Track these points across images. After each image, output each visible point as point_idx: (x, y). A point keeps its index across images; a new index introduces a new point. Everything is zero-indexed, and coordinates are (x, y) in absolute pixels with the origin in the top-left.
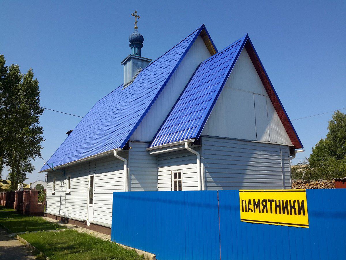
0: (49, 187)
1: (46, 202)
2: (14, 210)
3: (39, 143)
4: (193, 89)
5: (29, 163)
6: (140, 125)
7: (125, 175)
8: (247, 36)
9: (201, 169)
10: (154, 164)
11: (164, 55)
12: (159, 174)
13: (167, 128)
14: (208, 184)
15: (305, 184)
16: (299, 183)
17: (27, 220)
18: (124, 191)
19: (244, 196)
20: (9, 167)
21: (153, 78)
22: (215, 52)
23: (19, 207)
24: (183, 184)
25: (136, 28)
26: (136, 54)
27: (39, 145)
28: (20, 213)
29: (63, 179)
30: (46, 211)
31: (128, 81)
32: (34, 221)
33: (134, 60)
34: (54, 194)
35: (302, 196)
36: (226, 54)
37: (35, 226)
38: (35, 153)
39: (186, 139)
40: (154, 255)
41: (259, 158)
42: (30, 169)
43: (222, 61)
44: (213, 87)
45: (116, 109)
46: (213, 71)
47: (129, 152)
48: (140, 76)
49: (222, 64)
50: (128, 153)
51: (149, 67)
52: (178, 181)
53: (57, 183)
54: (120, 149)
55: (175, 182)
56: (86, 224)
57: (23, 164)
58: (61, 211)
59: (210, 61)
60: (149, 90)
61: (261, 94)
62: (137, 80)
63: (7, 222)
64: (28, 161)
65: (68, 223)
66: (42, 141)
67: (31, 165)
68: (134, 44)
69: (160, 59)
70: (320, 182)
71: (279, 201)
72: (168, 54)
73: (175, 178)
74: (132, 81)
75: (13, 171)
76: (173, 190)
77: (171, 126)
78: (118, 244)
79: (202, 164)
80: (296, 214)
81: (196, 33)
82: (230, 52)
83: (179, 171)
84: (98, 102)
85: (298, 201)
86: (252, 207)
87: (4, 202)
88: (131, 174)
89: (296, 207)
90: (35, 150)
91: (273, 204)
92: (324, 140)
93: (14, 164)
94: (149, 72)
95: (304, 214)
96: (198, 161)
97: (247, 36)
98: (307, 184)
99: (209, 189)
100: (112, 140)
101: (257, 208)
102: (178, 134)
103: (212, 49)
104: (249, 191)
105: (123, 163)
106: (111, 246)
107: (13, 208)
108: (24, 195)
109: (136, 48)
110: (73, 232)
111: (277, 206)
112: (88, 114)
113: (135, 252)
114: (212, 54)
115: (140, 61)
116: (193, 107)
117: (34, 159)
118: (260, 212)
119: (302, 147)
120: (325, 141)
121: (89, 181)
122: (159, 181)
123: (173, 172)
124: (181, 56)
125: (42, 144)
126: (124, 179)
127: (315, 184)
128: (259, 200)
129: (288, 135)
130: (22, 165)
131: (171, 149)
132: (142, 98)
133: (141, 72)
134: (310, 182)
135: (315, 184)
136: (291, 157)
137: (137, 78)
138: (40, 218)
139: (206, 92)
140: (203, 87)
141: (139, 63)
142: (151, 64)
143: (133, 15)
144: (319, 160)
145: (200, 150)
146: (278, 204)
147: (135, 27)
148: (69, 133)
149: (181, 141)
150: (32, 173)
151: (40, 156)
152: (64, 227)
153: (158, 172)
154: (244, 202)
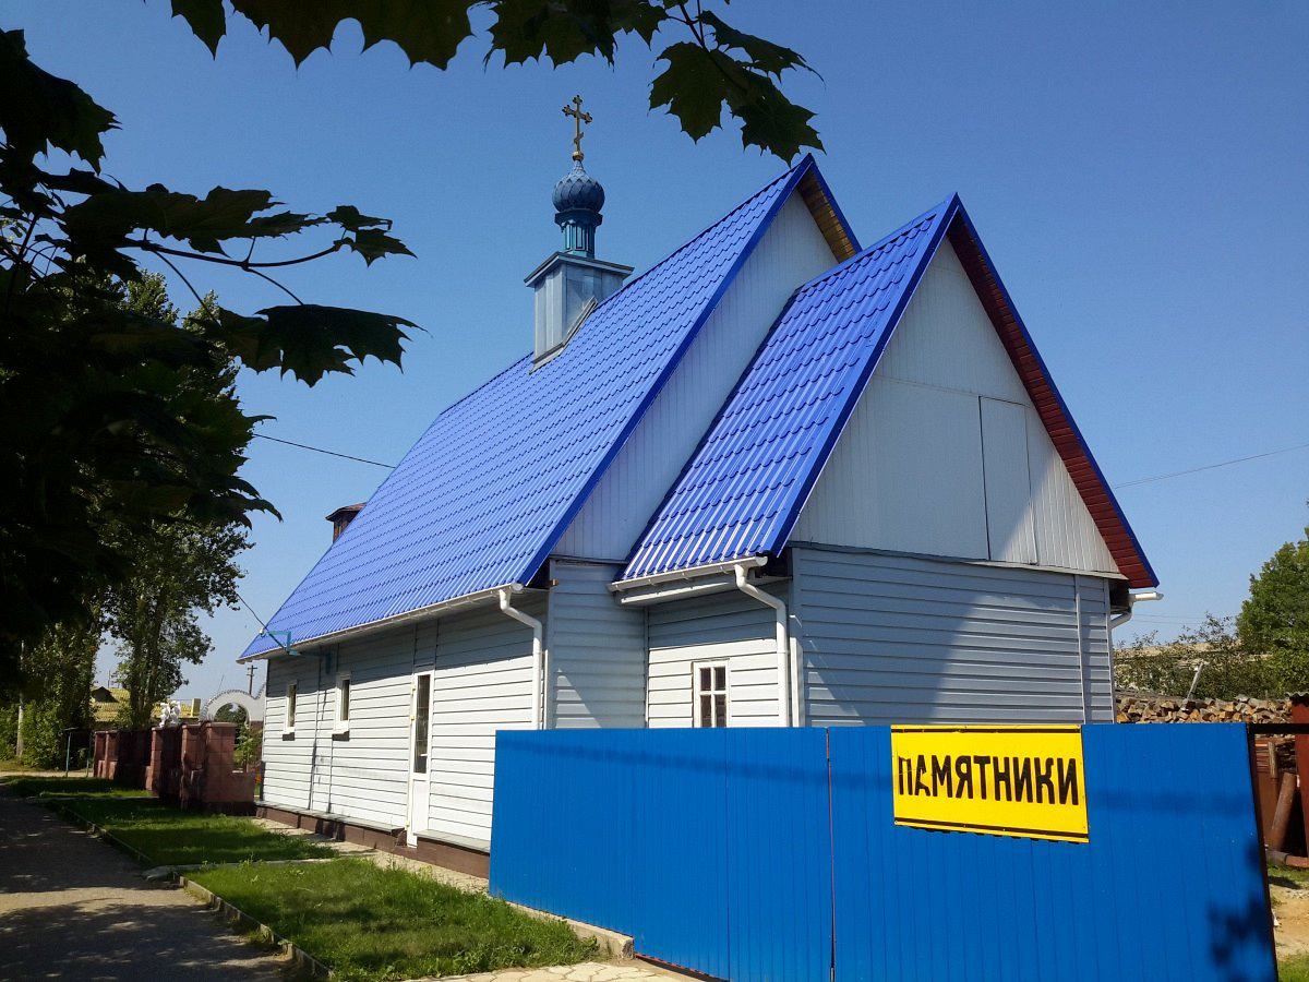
0: (273, 713)
1: (263, 764)
2: (148, 792)
3: (231, 553)
4: (828, 336)
5: (194, 627)
6: (587, 504)
7: (535, 674)
8: (956, 201)
9: (789, 655)
10: (637, 637)
11: (673, 256)
12: (652, 671)
13: (669, 518)
14: (815, 709)
15: (1188, 713)
16: (1167, 710)
17: (199, 826)
18: (533, 727)
19: (907, 745)
20: (120, 641)
21: (662, 297)
22: (849, 248)
23: (163, 783)
24: (731, 709)
25: (578, 158)
26: (578, 249)
27: (230, 562)
28: (168, 801)
29: (323, 685)
30: (261, 798)
31: (551, 345)
32: (222, 831)
33: (571, 270)
34: (290, 737)
35: (1068, 747)
36: (884, 260)
37: (231, 847)
38: (215, 591)
39: (741, 554)
40: (628, 938)
41: (992, 621)
42: (195, 647)
43: (870, 285)
44: (836, 377)
45: (507, 445)
46: (875, 283)
47: (560, 594)
48: (592, 326)
49: (869, 293)
50: (544, 599)
51: (621, 298)
52: (716, 696)
53: (301, 699)
54: (519, 588)
55: (706, 701)
56: (403, 842)
57: (172, 631)
58: (315, 797)
59: (829, 282)
60: (619, 384)
61: (1004, 398)
62: (581, 341)
63: (133, 831)
64: (188, 618)
65: (341, 838)
66: (241, 550)
67: (198, 633)
68: (573, 214)
69: (659, 270)
70: (1242, 708)
71: (1007, 760)
72: (687, 255)
73: (706, 685)
74: (561, 346)
75: (137, 654)
76: (698, 725)
77: (690, 508)
78: (513, 905)
79: (793, 641)
80: (1052, 801)
81: (782, 185)
82: (897, 253)
83: (719, 664)
84: (447, 414)
85: (1060, 761)
86: (927, 779)
87: (108, 764)
88: (555, 669)
89: (1054, 779)
90: (217, 579)
91: (989, 768)
92: (1296, 546)
93: (142, 633)
94: (620, 314)
95: (1075, 802)
96: (780, 629)
97: (956, 201)
98: (1194, 714)
99: (816, 723)
100: (514, 528)
101: (942, 783)
102: (715, 540)
103: (839, 241)
104: (920, 731)
105: (528, 633)
106: (490, 909)
107: (143, 787)
108: (184, 742)
109: (579, 229)
110: (359, 865)
111: (999, 777)
112: (410, 456)
113: (568, 929)
114: (840, 256)
115: (592, 272)
116: (767, 443)
117: (210, 610)
118: (950, 795)
119: (1154, 583)
120: (1297, 550)
121: (415, 693)
122: (652, 698)
123: (698, 666)
124: (728, 266)
125: (239, 560)
126: (534, 688)
127: (1223, 715)
128: (948, 759)
129: (1106, 540)
130: (168, 631)
131: (689, 589)
132: (596, 410)
133: (594, 311)
134: (1205, 707)
135: (1223, 715)
136: (1114, 617)
137: (581, 333)
138: (242, 820)
139: (812, 391)
140: (804, 374)
141: (589, 280)
142: (628, 286)
143: (567, 111)
144: (1276, 625)
145: (787, 591)
146: (1002, 770)
147: (576, 153)
148: (342, 518)
149: (722, 562)
150: (201, 662)
151: (235, 601)
152: (329, 853)
153: (646, 664)
154: (905, 764)
